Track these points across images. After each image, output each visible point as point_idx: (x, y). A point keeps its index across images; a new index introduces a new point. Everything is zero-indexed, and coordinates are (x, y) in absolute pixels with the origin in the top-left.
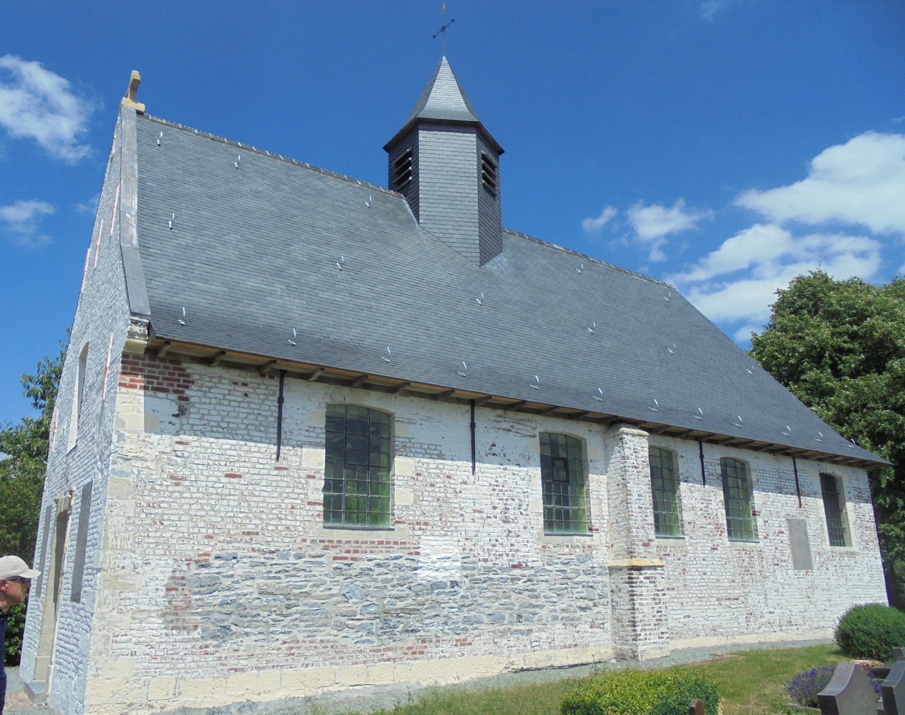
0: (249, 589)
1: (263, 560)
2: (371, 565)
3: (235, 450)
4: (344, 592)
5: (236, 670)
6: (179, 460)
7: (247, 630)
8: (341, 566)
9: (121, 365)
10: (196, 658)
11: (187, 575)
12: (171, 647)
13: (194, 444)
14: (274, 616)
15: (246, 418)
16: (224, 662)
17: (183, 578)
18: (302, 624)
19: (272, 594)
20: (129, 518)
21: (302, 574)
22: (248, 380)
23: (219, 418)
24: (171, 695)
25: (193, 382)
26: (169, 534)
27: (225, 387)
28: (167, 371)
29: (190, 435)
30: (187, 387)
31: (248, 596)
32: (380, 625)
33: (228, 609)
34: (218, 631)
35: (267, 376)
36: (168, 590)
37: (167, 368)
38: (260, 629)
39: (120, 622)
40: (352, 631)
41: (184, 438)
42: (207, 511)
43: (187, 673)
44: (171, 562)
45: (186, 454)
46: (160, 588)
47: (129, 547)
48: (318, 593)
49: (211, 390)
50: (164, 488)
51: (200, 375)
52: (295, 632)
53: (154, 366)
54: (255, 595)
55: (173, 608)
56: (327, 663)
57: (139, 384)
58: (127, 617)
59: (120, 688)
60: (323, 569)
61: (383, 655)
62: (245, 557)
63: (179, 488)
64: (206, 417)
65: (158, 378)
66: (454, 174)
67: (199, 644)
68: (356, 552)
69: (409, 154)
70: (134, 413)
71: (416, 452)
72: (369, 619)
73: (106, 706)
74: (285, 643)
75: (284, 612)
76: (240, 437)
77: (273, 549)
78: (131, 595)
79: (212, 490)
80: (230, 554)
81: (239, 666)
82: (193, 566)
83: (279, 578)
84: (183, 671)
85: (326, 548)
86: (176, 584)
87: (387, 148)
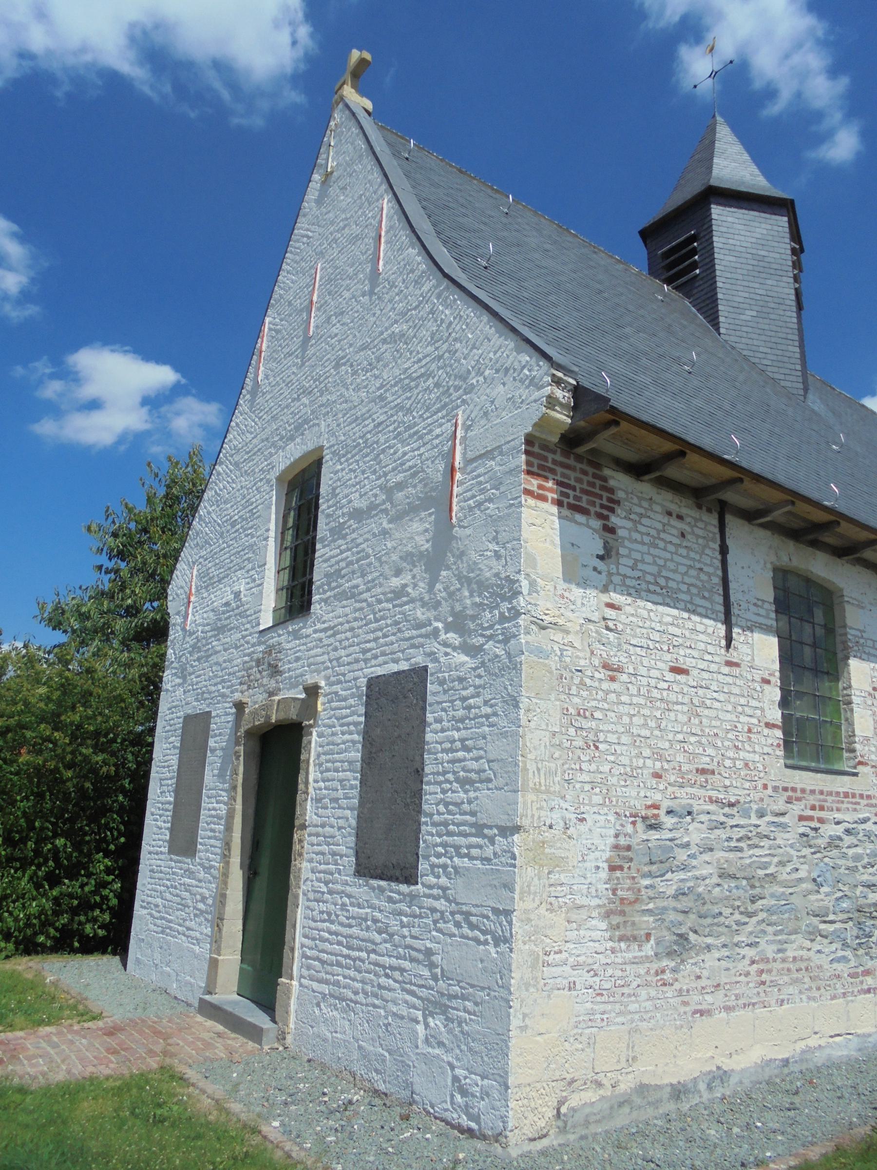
0: (706, 867)
1: (723, 819)
2: (839, 830)
3: (677, 626)
4: (814, 875)
5: (702, 1013)
6: (611, 635)
7: (709, 940)
8: (808, 831)
9: (524, 457)
10: (653, 993)
11: (634, 842)
12: (620, 973)
13: (629, 610)
14: (737, 916)
15: (686, 573)
16: (686, 999)
17: (629, 848)
18: (770, 929)
19: (734, 877)
20: (554, 734)
21: (765, 843)
22: (684, 511)
23: (654, 569)
24: (624, 1064)
25: (618, 502)
26: (606, 768)
27: (657, 519)
28: (585, 478)
29: (623, 594)
30: (612, 510)
31: (707, 881)
32: (855, 932)
33: (685, 903)
34: (676, 943)
35: (704, 508)
36: (612, 869)
37: (585, 473)
38: (723, 939)
39: (552, 927)
40: (826, 941)
41: (616, 598)
42: (651, 729)
43: (642, 1020)
44: (612, 818)
45: (620, 627)
46: (600, 865)
47: (557, 788)
48: (785, 876)
49: (647, 516)
50: (596, 684)
51: (627, 493)
52: (763, 944)
53: (568, 467)
54: (715, 880)
55: (618, 903)
56: (804, 997)
57: (550, 495)
58: (559, 919)
59: (555, 1051)
60: (787, 836)
61: (862, 982)
62: (702, 813)
63: (614, 686)
64: (640, 566)
65: (574, 489)
66: (762, 270)
67: (655, 966)
68: (822, 808)
69: (694, 238)
70: (547, 545)
71: (869, 654)
72: (843, 922)
73: (538, 1085)
74: (753, 962)
75: (750, 909)
76: (682, 605)
77: (733, 800)
78: (563, 878)
79: (655, 693)
80: (683, 807)
81: (704, 1007)
82: (640, 826)
83: (740, 850)
84: (637, 1017)
85: (789, 801)
86: (621, 859)
87: (646, 234)
